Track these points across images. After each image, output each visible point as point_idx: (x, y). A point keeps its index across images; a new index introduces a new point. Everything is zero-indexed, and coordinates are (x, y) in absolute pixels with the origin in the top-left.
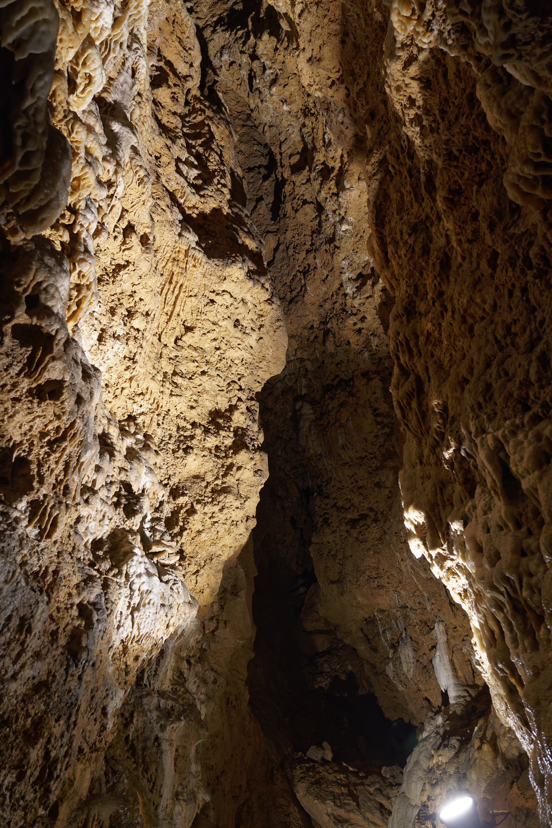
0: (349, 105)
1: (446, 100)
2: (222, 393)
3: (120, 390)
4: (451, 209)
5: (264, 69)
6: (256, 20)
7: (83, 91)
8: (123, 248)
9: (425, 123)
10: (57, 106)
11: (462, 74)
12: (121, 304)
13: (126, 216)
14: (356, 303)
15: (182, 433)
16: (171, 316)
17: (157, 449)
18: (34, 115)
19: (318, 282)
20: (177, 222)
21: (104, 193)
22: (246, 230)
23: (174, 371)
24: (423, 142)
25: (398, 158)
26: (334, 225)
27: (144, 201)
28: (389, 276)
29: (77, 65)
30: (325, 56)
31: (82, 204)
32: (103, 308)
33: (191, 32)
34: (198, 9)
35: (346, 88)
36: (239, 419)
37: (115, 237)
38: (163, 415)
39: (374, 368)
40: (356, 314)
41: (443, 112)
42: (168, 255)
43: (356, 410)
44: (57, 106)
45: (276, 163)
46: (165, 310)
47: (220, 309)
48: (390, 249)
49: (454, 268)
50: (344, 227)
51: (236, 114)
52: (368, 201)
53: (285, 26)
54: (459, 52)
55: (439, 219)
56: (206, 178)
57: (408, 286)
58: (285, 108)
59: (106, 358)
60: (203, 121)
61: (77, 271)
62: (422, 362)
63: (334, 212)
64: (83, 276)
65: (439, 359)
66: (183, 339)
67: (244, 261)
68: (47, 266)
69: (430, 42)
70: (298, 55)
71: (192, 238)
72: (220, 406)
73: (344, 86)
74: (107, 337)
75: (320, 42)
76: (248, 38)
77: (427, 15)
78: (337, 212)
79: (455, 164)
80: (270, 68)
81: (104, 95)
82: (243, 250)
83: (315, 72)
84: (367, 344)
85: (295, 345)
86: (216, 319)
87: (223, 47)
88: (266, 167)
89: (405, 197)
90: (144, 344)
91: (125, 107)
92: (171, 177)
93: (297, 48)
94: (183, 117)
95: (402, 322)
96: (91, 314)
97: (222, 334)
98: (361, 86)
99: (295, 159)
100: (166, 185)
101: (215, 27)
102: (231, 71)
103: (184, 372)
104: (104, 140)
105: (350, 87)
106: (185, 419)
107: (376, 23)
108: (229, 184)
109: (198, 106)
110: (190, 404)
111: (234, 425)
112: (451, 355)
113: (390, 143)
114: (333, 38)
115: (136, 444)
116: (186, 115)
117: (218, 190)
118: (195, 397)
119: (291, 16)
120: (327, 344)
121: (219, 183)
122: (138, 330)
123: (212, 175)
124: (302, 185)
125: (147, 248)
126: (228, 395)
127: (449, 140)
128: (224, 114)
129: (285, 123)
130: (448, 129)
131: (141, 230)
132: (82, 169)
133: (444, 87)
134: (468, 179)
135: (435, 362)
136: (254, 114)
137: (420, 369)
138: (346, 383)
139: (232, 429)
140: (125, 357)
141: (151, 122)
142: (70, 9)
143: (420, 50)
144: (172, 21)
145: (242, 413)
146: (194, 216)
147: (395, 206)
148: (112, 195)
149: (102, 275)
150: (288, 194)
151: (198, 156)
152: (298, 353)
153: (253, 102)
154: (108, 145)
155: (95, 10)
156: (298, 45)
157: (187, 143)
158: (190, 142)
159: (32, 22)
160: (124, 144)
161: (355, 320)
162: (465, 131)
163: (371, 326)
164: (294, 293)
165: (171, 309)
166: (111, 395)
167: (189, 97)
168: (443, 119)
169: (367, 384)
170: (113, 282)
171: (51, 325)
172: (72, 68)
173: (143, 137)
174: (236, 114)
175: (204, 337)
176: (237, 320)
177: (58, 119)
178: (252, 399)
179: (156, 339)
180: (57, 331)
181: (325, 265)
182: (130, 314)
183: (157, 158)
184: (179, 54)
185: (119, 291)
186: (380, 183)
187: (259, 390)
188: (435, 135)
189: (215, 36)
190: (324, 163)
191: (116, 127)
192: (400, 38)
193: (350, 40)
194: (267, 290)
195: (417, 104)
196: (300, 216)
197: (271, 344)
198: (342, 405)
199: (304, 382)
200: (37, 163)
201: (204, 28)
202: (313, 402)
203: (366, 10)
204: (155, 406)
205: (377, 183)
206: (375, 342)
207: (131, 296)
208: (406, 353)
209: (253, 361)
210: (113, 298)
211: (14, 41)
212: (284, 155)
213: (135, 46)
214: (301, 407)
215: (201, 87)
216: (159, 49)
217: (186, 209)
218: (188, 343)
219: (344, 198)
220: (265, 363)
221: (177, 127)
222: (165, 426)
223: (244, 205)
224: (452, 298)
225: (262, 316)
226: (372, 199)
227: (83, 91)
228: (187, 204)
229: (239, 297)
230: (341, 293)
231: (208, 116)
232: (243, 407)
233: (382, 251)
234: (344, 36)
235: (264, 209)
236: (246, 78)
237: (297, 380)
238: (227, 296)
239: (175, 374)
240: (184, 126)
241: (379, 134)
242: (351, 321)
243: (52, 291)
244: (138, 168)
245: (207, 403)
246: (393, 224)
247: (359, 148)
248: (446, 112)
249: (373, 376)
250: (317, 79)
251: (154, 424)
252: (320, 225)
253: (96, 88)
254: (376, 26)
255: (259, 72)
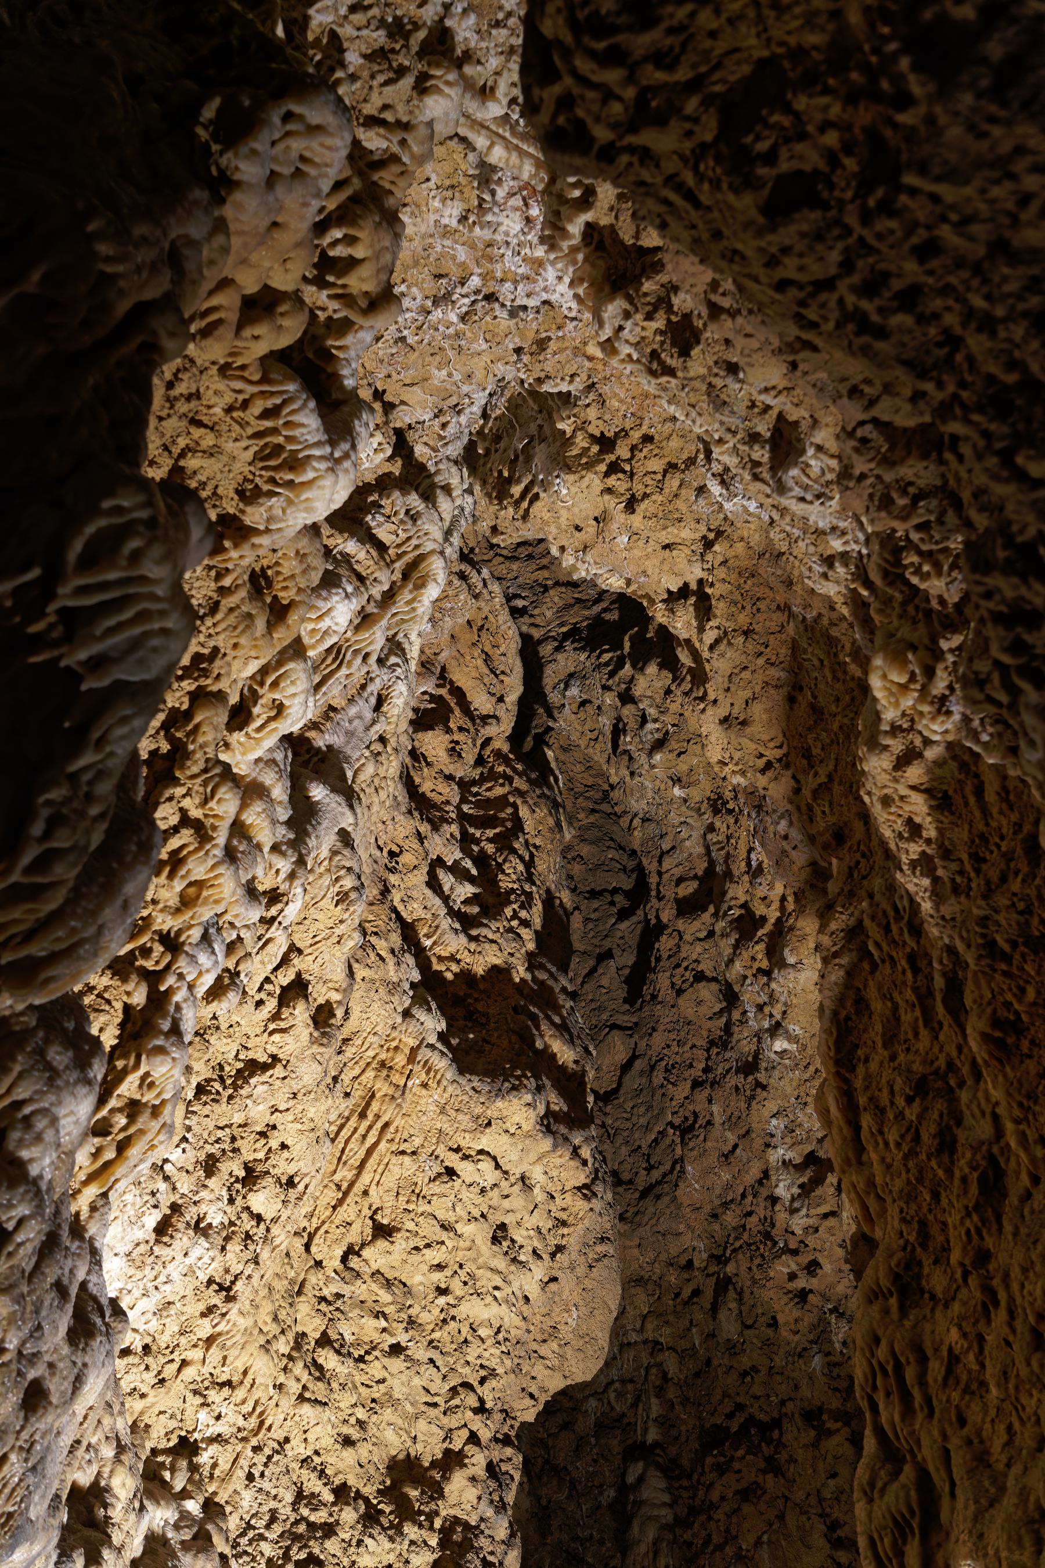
0: (798, 808)
1: (982, 836)
2: (433, 1412)
3: (175, 1366)
4: (1000, 1061)
5: (644, 720)
6: (639, 641)
7: (259, 729)
8: (272, 1026)
9: (940, 872)
10: (194, 752)
11: (1012, 797)
12: (235, 1150)
13: (296, 961)
14: (798, 1223)
15: (305, 1512)
16: (346, 1194)
17: (227, 1550)
18: (91, 783)
19: (712, 1159)
20: (406, 986)
21: (255, 914)
22: (557, 1020)
23: (324, 1334)
24: (937, 907)
25: (887, 929)
26: (757, 1035)
27: (340, 937)
28: (861, 1186)
29: (262, 684)
30: (756, 717)
31: (196, 934)
32: (191, 1154)
33: (511, 644)
34: (536, 612)
35: (794, 777)
36: (462, 1496)
37: (260, 1003)
38: (267, 1451)
39: (835, 1403)
40: (795, 1252)
41: (977, 860)
42: (371, 1053)
43: (781, 1517)
44: (194, 752)
45: (649, 890)
46: (337, 1177)
47: (465, 1195)
48: (867, 1121)
49: (1013, 1200)
50: (780, 1045)
51: (580, 788)
52: (821, 1008)
53: (684, 657)
54: (1003, 758)
55: (978, 1076)
56: (491, 902)
57: (903, 1220)
58: (677, 792)
59: (162, 1278)
60: (504, 797)
61: (141, 1072)
62: (936, 1433)
63: (760, 1008)
64: (151, 1085)
65: (979, 1432)
66: (366, 1253)
67: (539, 1089)
68: (49, 1067)
69: (946, 732)
70: (703, 710)
71: (432, 1023)
72: (419, 1447)
73: (789, 773)
74: (181, 1226)
75: (747, 694)
76: (620, 665)
77: (940, 686)
78: (767, 1010)
79: (1004, 967)
80: (655, 721)
81: (311, 734)
82: (543, 1065)
83: (734, 742)
84: (821, 1335)
85: (642, 1301)
86: (451, 1217)
87: (571, 675)
88: (627, 894)
89: (902, 1011)
90: (265, 1255)
91: (347, 759)
92: (415, 894)
93: (702, 699)
94: (464, 785)
95: (886, 1311)
96: (158, 1168)
97: (460, 1256)
98: (823, 779)
99: (689, 888)
100: (400, 908)
101: (561, 642)
102: (582, 715)
103: (348, 1337)
104: (283, 814)
105: (800, 777)
106: (322, 1474)
107: (853, 678)
108: (537, 922)
109: (501, 769)
110: (346, 1430)
111: (445, 1510)
112: (1009, 1428)
113: (871, 896)
114: (773, 692)
115: (177, 1527)
116: (474, 783)
117: (511, 930)
118: (361, 1414)
119: (697, 645)
120: (722, 1315)
121: (515, 916)
122: (259, 1218)
123: (504, 898)
124: (696, 943)
125: (324, 1034)
126: (445, 1421)
127: (986, 918)
128: (550, 787)
129: (674, 818)
130: (985, 897)
131: (320, 994)
132: (213, 867)
133: (977, 814)
134: (1035, 1004)
135: (969, 1442)
136: (615, 795)
137: (928, 1453)
138: (763, 1431)
139: (438, 1523)
140: (210, 1282)
141: (395, 789)
142: (269, 600)
143: (927, 742)
144: (479, 627)
145: (473, 1479)
146: (449, 976)
147: (879, 1027)
148: (273, 919)
149: (208, 1081)
150: (665, 955)
151: (481, 860)
152: (649, 1326)
153: (616, 773)
154: (289, 823)
155: (320, 603)
156: (705, 693)
157: (464, 833)
158: (472, 830)
159: (136, 631)
160: (325, 823)
161: (794, 1267)
162: (1021, 906)
163: (831, 1286)
164: (656, 1175)
165: (350, 1175)
166: (150, 1378)
167: (487, 752)
168: (978, 871)
169: (815, 1445)
170: (230, 1098)
171: (10, 1206)
172: (250, 688)
173: (378, 815)
174: (581, 789)
175: (416, 1258)
176: (503, 1227)
177: (189, 773)
178: (506, 1441)
179: (299, 1244)
180: (20, 1222)
181: (732, 1121)
182: (251, 1177)
183: (392, 854)
184: (481, 678)
185: (238, 1118)
186: (848, 974)
187: (530, 1417)
188: (963, 898)
189: (560, 657)
190: (744, 906)
191: (318, 792)
192: (890, 715)
193: (805, 698)
194: (585, 1163)
195: (925, 834)
196: (686, 1006)
197: (576, 1298)
198: (746, 1494)
199: (656, 1408)
200: (66, 872)
201: (540, 642)
202: (671, 1471)
203: (836, 655)
204: (253, 1422)
205: (842, 973)
206: (840, 1331)
207: (263, 1134)
208: (895, 1398)
209: (527, 1338)
210: (220, 1134)
211: (90, 658)
212: (666, 877)
213: (393, 660)
214: (641, 1479)
215: (516, 738)
216: (444, 669)
217: (434, 960)
218: (375, 1267)
219: (784, 983)
220: (554, 1346)
221: (448, 802)
222: (266, 1485)
223: (564, 968)
224: (1006, 1277)
225: (564, 1224)
226: (827, 1003)
227: (259, 729)
228: (437, 950)
229: (516, 1172)
230: (764, 1192)
231: (517, 789)
232: (478, 1460)
233: (849, 1122)
234: (793, 692)
235: (610, 976)
236: (608, 730)
237: (638, 1399)
238: (486, 1165)
239: (324, 1341)
240: (463, 800)
241: (850, 875)
242: (784, 1266)
243: (40, 1124)
244: (342, 872)
245: (390, 1435)
246: (873, 1066)
247: (815, 889)
248: (984, 860)
249: (831, 1425)
250: (737, 755)
251: (241, 1474)
252: (728, 1028)
253: (293, 723)
254: (852, 685)
255: (632, 724)
